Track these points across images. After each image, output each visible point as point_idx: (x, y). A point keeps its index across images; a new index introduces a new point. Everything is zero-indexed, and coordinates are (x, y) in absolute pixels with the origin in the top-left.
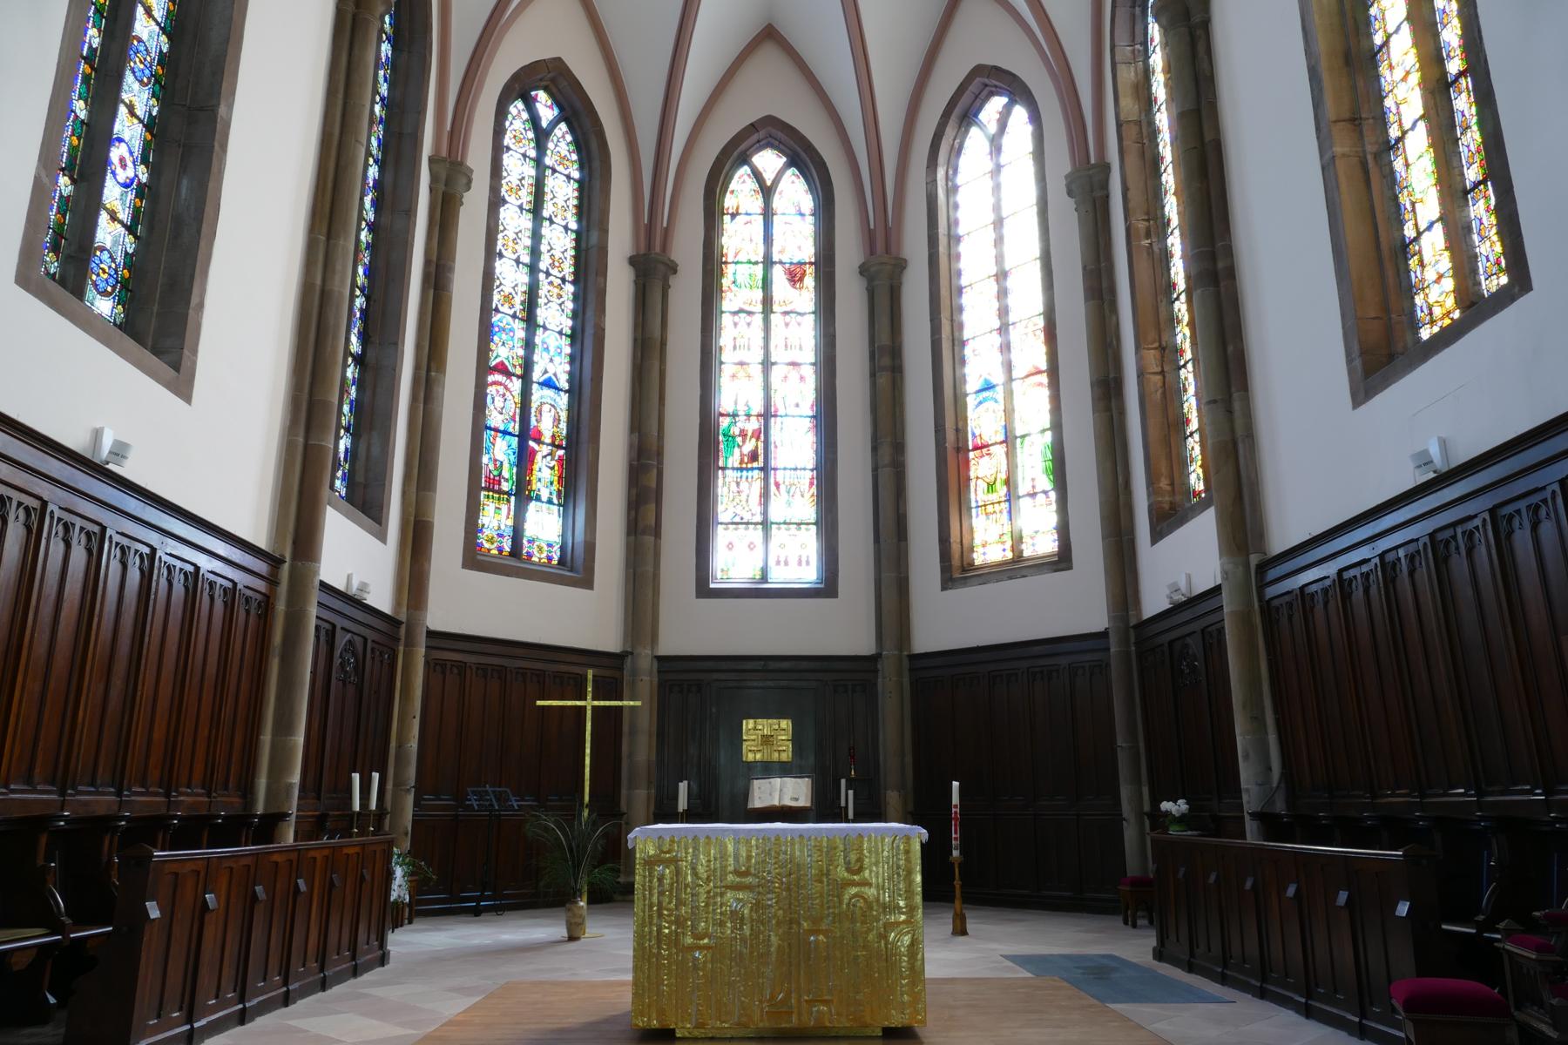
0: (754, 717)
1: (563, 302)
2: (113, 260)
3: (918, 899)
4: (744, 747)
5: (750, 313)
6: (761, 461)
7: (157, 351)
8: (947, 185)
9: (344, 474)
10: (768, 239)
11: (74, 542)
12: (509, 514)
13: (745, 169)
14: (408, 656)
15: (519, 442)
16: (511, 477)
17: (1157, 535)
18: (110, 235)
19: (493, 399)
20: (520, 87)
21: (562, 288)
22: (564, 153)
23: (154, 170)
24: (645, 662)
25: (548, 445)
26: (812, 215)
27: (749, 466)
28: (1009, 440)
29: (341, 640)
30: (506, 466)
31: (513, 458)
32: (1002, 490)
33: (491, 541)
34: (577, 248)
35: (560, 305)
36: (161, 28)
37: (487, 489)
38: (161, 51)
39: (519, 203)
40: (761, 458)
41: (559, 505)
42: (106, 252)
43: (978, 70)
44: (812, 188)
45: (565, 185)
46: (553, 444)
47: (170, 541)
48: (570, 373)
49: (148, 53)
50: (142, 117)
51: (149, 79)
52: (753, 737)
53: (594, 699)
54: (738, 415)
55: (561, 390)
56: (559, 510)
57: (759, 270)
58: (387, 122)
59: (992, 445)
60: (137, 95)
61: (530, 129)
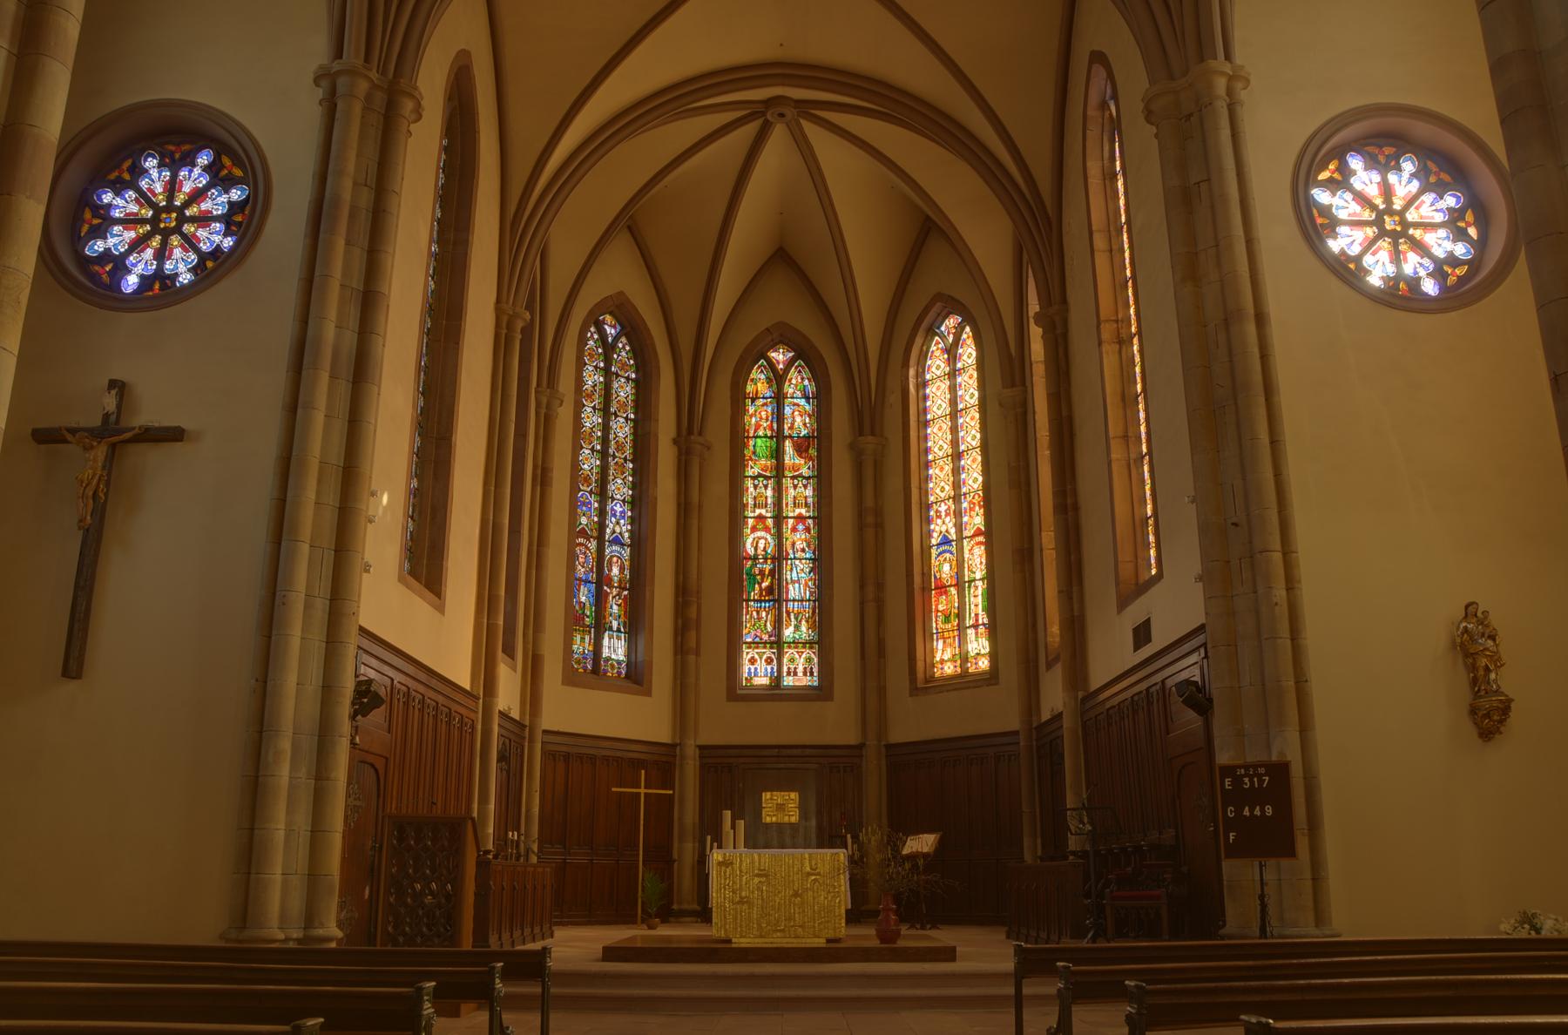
0: (772, 791)
4: (763, 813)
6: (776, 595)
10: (779, 416)
12: (590, 641)
14: (531, 749)
15: (596, 588)
24: (691, 751)
25: (616, 587)
27: (767, 598)
30: (587, 605)
33: (578, 662)
34: (635, 433)
35: (623, 480)
41: (625, 633)
43: (938, 297)
46: (619, 587)
48: (631, 531)
52: (770, 805)
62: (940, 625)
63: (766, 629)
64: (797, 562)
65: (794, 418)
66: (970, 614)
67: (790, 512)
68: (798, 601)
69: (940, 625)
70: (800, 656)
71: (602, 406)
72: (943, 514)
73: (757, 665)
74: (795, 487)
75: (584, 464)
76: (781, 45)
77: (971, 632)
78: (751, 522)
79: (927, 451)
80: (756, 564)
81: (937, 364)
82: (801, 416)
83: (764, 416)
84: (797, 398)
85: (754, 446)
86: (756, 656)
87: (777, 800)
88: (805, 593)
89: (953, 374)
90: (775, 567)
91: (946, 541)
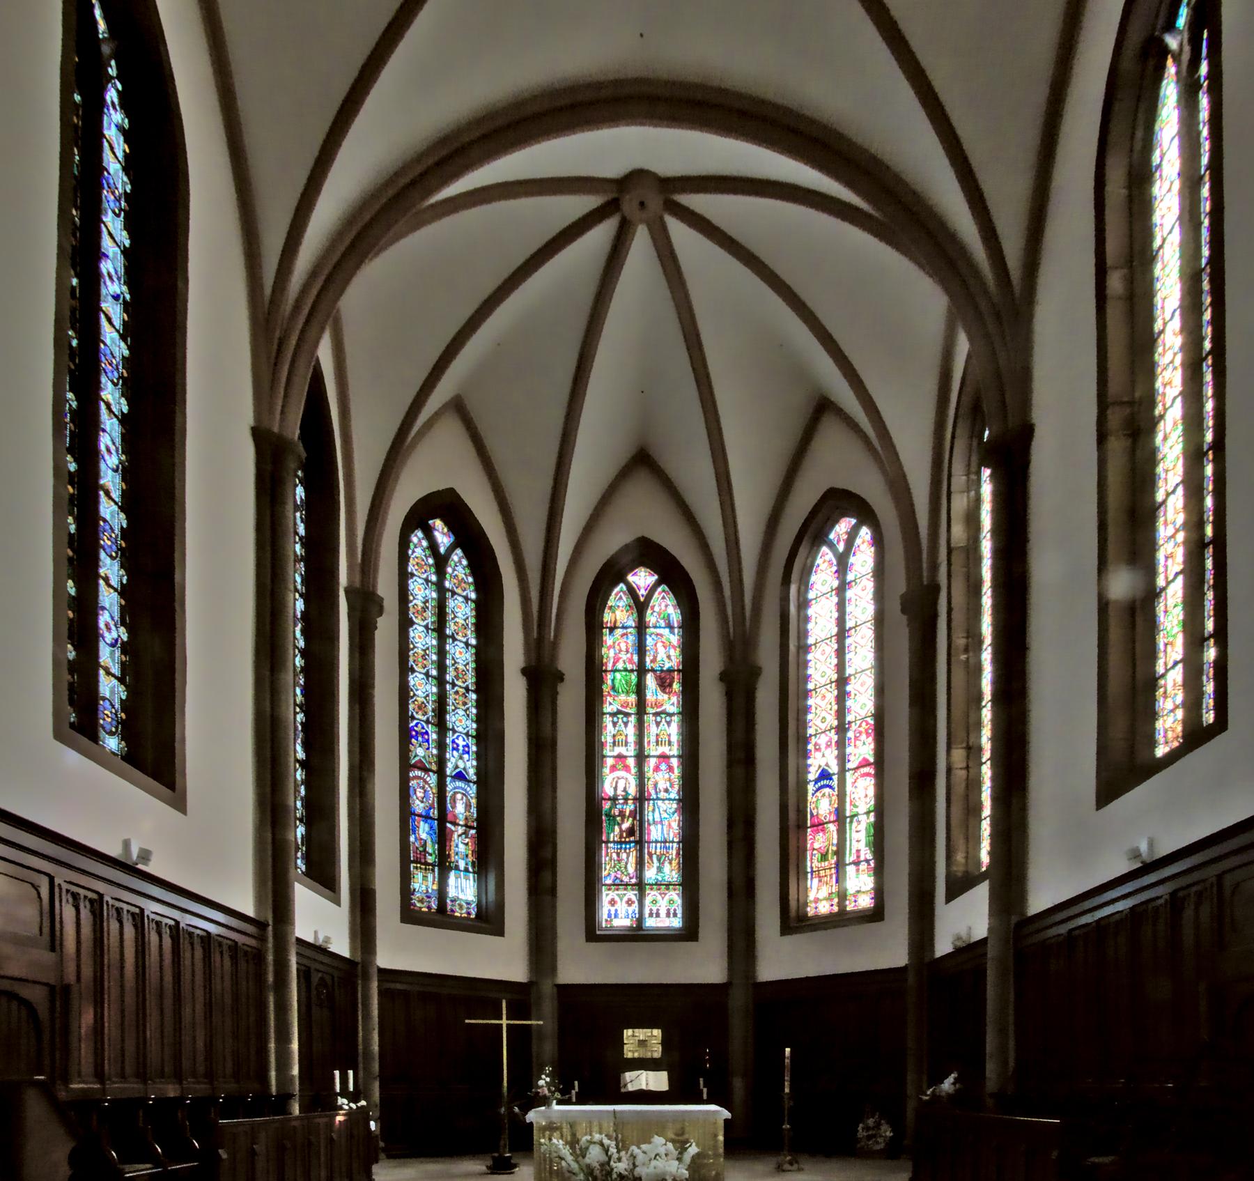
1: (468, 709)
2: (113, 707)
3: (721, 1150)
5: (627, 715)
6: (637, 836)
7: (156, 776)
8: (798, 599)
9: (302, 854)
10: (641, 649)
11: (125, 921)
12: (434, 880)
13: (622, 586)
16: (434, 852)
17: (951, 896)
18: (110, 688)
19: (415, 790)
20: (418, 518)
21: (466, 697)
22: (461, 576)
23: (130, 631)
24: (547, 988)
25: (462, 826)
26: (680, 628)
27: (627, 840)
28: (841, 818)
29: (315, 978)
30: (429, 844)
31: (435, 837)
32: (833, 860)
33: (421, 901)
35: (466, 711)
36: (119, 507)
37: (416, 862)
38: (122, 527)
39: (425, 623)
40: (637, 834)
41: (474, 873)
42: (107, 701)
44: (680, 604)
45: (463, 606)
47: (188, 916)
48: (478, 768)
49: (113, 530)
50: (116, 586)
51: (116, 553)
53: (507, 1025)
54: (618, 799)
55: (471, 782)
56: (474, 877)
57: (634, 677)
58: (306, 559)
59: (827, 823)
60: (111, 569)
61: (430, 556)
62: (815, 864)
63: (627, 870)
64: (660, 802)
65: (657, 650)
66: (851, 850)
67: (653, 750)
68: (661, 842)
69: (815, 864)
70: (663, 898)
71: (436, 626)
72: (823, 747)
73: (618, 906)
74: (658, 724)
75: (417, 690)
76: (642, 35)
77: (851, 870)
78: (610, 762)
79: (807, 678)
80: (616, 805)
81: (823, 577)
82: (665, 647)
83: (624, 648)
84: (660, 627)
85: (613, 680)
86: (617, 898)
87: (639, 1036)
88: (668, 834)
89: (841, 589)
90: (636, 807)
91: (824, 775)
